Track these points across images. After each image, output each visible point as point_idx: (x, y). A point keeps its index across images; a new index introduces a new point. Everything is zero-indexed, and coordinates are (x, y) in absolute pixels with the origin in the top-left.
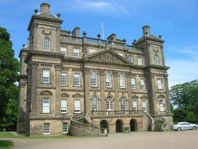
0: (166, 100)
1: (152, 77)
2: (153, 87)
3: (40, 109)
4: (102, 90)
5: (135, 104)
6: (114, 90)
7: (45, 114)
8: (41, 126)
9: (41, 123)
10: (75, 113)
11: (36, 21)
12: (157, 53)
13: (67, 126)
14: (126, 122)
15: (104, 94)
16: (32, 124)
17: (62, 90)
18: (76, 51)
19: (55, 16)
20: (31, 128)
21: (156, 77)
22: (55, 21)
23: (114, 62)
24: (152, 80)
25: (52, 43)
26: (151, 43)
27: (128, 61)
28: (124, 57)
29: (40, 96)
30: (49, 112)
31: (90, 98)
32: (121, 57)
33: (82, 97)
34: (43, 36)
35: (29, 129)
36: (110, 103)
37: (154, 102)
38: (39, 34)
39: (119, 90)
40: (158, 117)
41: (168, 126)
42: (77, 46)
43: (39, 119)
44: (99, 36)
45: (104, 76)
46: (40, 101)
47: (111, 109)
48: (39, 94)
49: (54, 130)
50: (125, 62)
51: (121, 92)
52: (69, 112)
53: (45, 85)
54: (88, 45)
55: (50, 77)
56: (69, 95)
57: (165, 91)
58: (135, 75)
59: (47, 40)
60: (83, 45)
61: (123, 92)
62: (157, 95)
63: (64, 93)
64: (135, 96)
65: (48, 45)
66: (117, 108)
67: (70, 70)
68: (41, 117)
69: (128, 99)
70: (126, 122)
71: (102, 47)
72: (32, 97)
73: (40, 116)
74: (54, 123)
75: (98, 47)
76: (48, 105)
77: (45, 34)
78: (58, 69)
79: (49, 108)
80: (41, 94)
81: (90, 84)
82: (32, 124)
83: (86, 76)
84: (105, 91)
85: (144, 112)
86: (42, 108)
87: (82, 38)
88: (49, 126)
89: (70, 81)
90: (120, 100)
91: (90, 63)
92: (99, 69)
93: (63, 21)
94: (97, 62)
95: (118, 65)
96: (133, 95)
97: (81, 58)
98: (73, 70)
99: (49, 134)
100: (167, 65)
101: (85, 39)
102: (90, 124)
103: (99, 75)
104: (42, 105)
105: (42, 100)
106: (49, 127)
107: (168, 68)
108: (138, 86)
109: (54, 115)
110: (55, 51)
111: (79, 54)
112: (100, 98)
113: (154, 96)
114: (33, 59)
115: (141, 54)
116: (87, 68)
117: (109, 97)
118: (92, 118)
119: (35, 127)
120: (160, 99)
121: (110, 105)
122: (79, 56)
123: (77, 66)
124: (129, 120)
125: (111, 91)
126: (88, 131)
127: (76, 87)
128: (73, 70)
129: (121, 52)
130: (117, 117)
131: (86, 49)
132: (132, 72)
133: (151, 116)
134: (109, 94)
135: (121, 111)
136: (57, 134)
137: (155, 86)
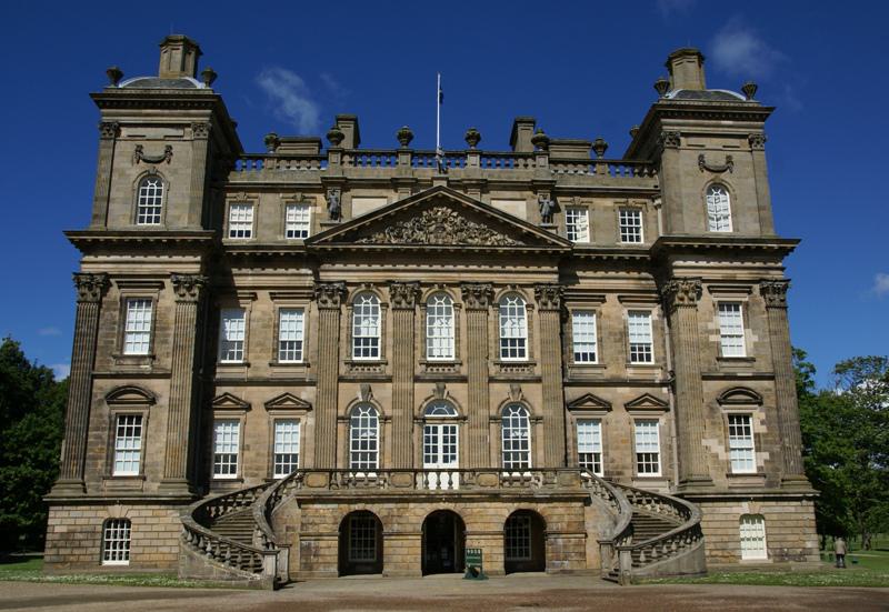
0: (774, 413)
3: (100, 462)
5: (589, 439)
7: (121, 483)
9: (94, 517)
14: (485, 526)
16: (58, 521)
19: (732, 93)
20: (49, 537)
26: (685, 129)
29: (106, 409)
30: (136, 473)
36: (440, 435)
38: (122, 165)
42: (299, 195)
46: (104, 429)
48: (100, 402)
49: (147, 550)
53: (129, 362)
55: (154, 328)
57: (658, 376)
63: (226, 394)
64: (591, 398)
67: (263, 295)
70: (485, 526)
72: (69, 415)
74: (149, 521)
75: (394, 184)
77: (145, 161)
79: (137, 456)
80: (113, 397)
82: (58, 521)
92: (388, 283)
94: (426, 254)
95: (491, 257)
96: (574, 393)
108: (612, 349)
114: (675, 271)
120: (725, 410)
121: (440, 444)
125: (448, 380)
129: (517, 194)
136: (156, 566)
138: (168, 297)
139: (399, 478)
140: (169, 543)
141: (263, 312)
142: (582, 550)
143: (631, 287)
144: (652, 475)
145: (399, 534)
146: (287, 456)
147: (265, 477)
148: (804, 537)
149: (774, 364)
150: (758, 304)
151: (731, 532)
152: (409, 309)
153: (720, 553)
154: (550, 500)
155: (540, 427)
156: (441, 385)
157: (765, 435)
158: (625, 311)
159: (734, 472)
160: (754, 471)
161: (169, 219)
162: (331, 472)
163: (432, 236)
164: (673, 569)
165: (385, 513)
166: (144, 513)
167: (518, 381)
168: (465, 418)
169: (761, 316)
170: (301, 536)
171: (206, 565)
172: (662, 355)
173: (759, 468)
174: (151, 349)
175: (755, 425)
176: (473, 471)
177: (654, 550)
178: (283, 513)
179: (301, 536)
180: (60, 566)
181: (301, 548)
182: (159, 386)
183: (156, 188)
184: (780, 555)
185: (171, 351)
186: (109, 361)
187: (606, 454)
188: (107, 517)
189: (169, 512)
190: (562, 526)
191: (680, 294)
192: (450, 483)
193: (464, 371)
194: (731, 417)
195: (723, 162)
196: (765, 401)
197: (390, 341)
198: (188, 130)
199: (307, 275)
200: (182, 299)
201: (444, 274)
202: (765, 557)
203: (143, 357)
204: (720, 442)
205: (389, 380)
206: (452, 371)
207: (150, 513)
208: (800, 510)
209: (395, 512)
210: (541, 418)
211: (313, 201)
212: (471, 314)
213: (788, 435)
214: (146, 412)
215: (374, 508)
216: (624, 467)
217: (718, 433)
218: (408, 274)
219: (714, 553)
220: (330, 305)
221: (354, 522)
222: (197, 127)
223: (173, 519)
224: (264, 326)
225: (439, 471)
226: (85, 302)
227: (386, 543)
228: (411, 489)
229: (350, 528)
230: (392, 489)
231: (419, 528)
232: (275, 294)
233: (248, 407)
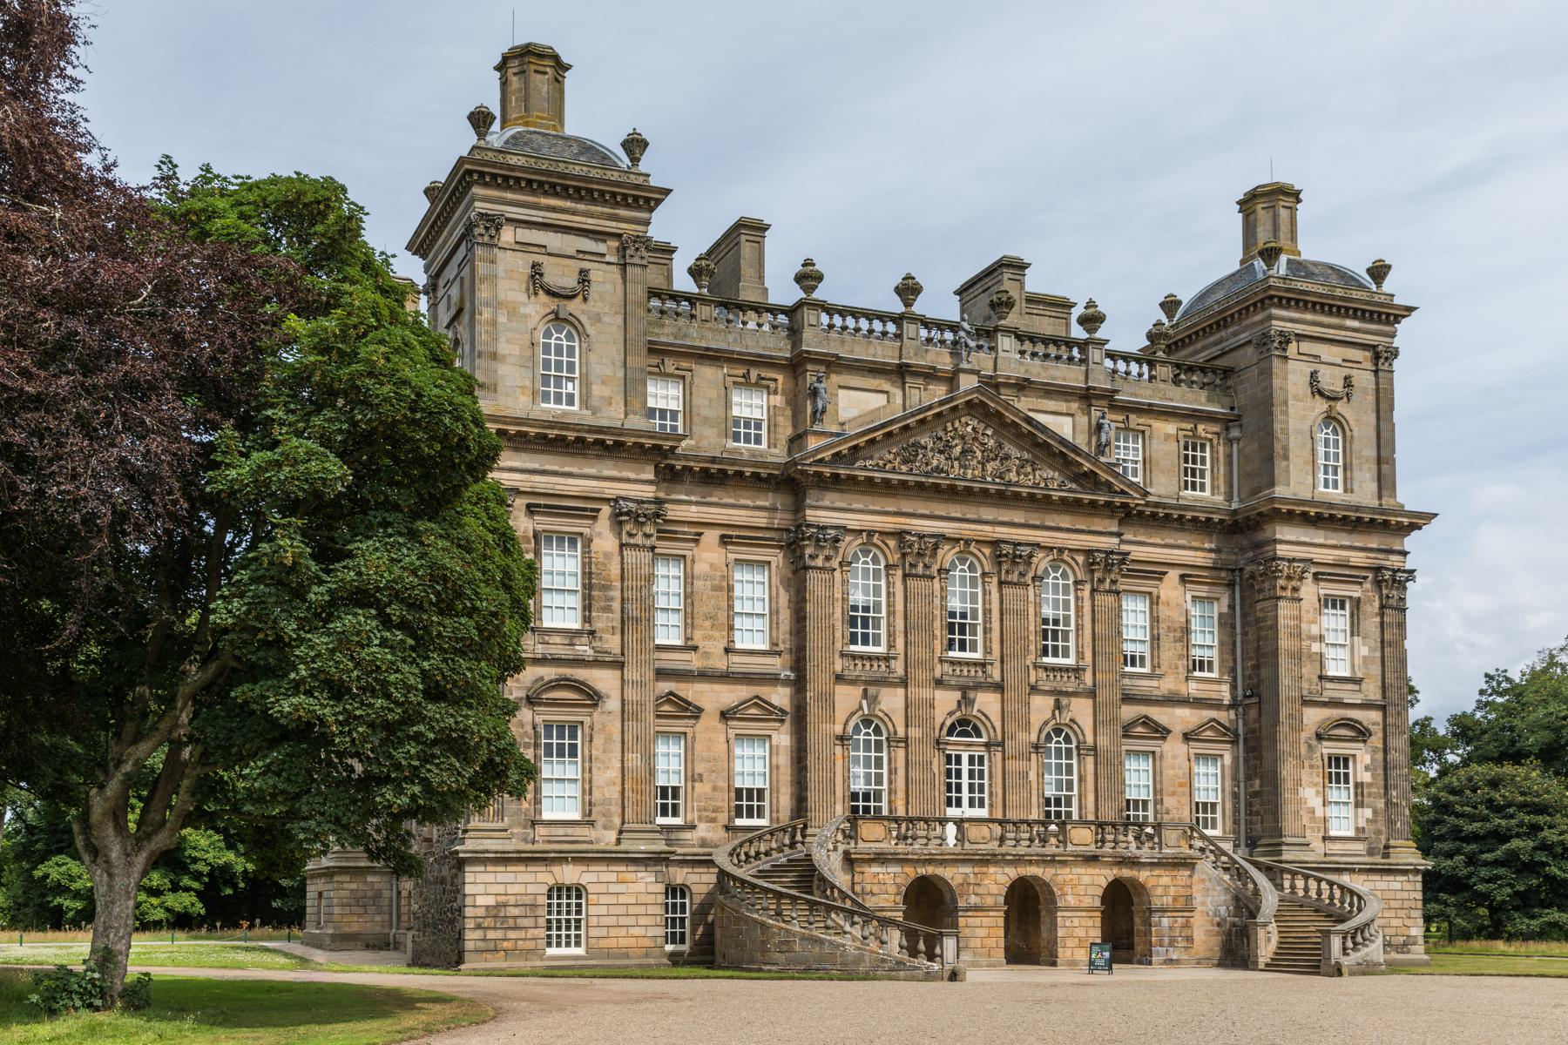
0: (1380, 756)
1: (1283, 588)
2: (1283, 661)
4: (919, 674)
5: (1137, 779)
6: (997, 676)
8: (534, 906)
9: (535, 881)
10: (739, 822)
11: (483, 201)
12: (1340, 407)
13: (683, 905)
15: (932, 706)
16: (479, 889)
17: (661, 674)
18: (750, 405)
20: (469, 912)
21: (1310, 591)
22: (614, 195)
23: (1009, 483)
24: (1285, 610)
25: (593, 358)
26: (1300, 328)
27: (1110, 468)
28: (1081, 441)
30: (576, 816)
31: (838, 729)
32: (1063, 441)
33: (782, 721)
34: (537, 308)
35: (452, 922)
36: (965, 767)
37: (1287, 771)
39: (1033, 680)
40: (1306, 877)
41: (1379, 941)
42: (754, 374)
43: (520, 860)
45: (936, 581)
47: (971, 805)
49: (613, 932)
50: (1089, 480)
51: (1047, 693)
52: (700, 819)
53: (558, 639)
54: (834, 364)
55: (588, 587)
56: (700, 710)
58: (1155, 572)
59: (559, 338)
60: (796, 365)
61: (1058, 693)
62: (1314, 717)
64: (1147, 721)
65: (571, 366)
66: (1012, 798)
67: (711, 536)
68: (529, 847)
69: (1090, 740)
71: (931, 375)
73: (525, 841)
74: (614, 888)
75: (901, 373)
76: (571, 770)
77: (549, 292)
79: (574, 790)
81: (838, 634)
82: (479, 889)
83: (814, 580)
84: (939, 683)
85: (1203, 837)
87: (792, 311)
88: (579, 905)
90: (1036, 747)
91: (842, 491)
92: (900, 535)
93: (667, 192)
95: (1039, 502)
96: (1129, 712)
97: (779, 455)
98: (725, 541)
99: (581, 951)
100: (1409, 496)
101: (809, 316)
102: (844, 896)
103: (899, 573)
106: (579, 912)
107: (1417, 521)
108: (1169, 652)
109: (612, 836)
110: (612, 415)
111: (765, 426)
112: (901, 732)
113: (1284, 728)
115: (1209, 418)
116: (824, 528)
117: (963, 722)
118: (849, 861)
119: (498, 906)
120: (1328, 748)
121: (965, 781)
122: (764, 446)
123: (750, 511)
124: (1097, 879)
125: (978, 687)
126: (838, 939)
128: (725, 541)
129: (1062, 406)
130: (1018, 860)
131: (814, 393)
132: (1138, 552)
133: (1256, 865)
134: (966, 701)
135: (1044, 824)
136: (627, 956)
137: (1298, 657)
140: (643, 921)
143: (1200, 562)
145: (977, 908)
146: (750, 791)
147: (726, 822)
148: (1407, 922)
159: (1332, 833)
165: (959, 879)
166: (605, 877)
174: (587, 619)
180: (489, 956)
182: (604, 680)
188: (551, 882)
189: (640, 875)
190: (1167, 901)
191: (1281, 582)
201: (973, 526)
207: (613, 877)
209: (972, 879)
211: (772, 385)
213: (1396, 787)
218: (926, 521)
220: (639, 540)
224: (715, 588)
231: (1001, 900)
232: (731, 537)
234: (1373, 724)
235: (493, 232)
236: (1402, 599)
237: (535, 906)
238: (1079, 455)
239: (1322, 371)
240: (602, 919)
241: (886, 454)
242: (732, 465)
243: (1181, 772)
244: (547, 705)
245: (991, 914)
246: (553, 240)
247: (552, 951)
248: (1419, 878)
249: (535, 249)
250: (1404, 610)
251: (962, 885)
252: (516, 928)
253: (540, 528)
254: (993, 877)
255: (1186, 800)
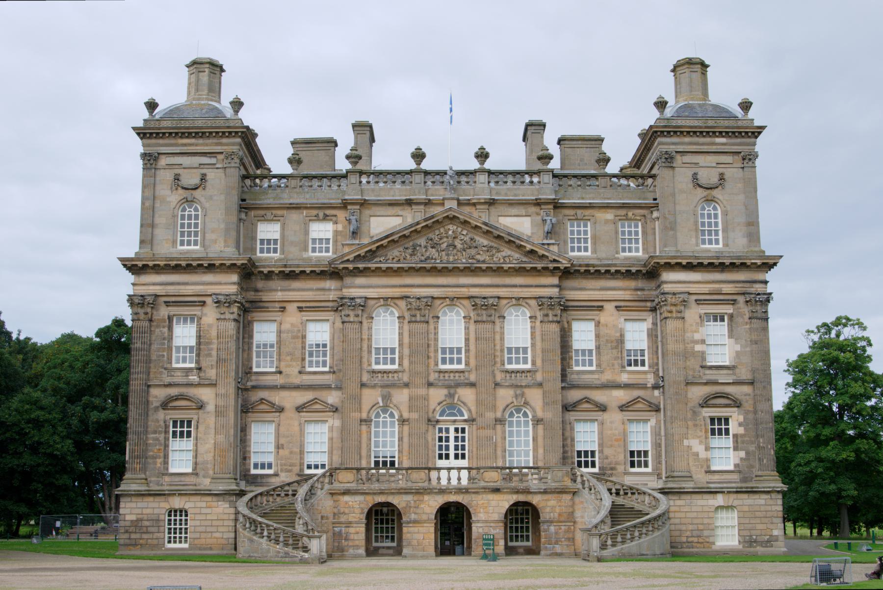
0: (751, 416)
7: (177, 479)
8: (158, 520)
9: (158, 508)
18: (322, 230)
26: (680, 148)
29: (161, 415)
30: (189, 470)
44: (419, 156)
46: (160, 432)
48: (156, 409)
49: (203, 535)
55: (199, 343)
64: (588, 400)
67: (292, 308)
73: (158, 484)
74: (204, 511)
76: (187, 444)
78: (228, 316)
79: (190, 456)
80: (165, 405)
86: (166, 457)
89: (290, 354)
98: (300, 309)
99: (186, 546)
100: (769, 249)
104: (166, 446)
105: (167, 427)
108: (608, 355)
116: (353, 299)
119: (138, 520)
120: (708, 413)
122: (721, 246)
127: (315, 373)
136: (211, 549)
138: (210, 315)
139: (415, 475)
140: (221, 529)
141: (292, 325)
142: (571, 536)
144: (643, 470)
145: (415, 522)
149: (753, 371)
150: (742, 315)
151: (706, 521)
152: (423, 322)
153: (695, 540)
154: (545, 492)
155: (540, 428)
156: (452, 391)
157: (742, 436)
158: (622, 320)
159: (713, 468)
160: (731, 468)
161: (207, 243)
162: (358, 470)
163: (444, 253)
164: (635, 551)
165: (408, 506)
167: (521, 386)
168: (473, 420)
169: (743, 329)
170: (333, 523)
171: (264, 546)
172: (655, 361)
173: (736, 465)
174: (198, 362)
175: (734, 427)
176: (478, 469)
177: (628, 533)
178: (318, 504)
179: (333, 523)
181: (334, 534)
182: (206, 394)
183: (193, 213)
184: (749, 541)
185: (214, 363)
186: (161, 373)
187: (601, 451)
188: (168, 507)
189: (220, 503)
192: (459, 479)
193: (473, 378)
194: (712, 420)
195: (715, 180)
196: (745, 404)
197: (406, 351)
198: (220, 157)
199: (330, 290)
200: (222, 317)
201: (454, 289)
202: (737, 543)
203: (191, 369)
204: (701, 442)
205: (407, 385)
206: (462, 378)
207: (204, 504)
208: (771, 502)
210: (542, 420)
211: (334, 219)
212: (480, 326)
213: (763, 436)
214: (195, 417)
215: (395, 500)
216: (617, 463)
217: (700, 434)
219: (690, 539)
221: (376, 512)
222: (230, 156)
223: (223, 508)
224: (294, 337)
225: (449, 469)
226: (139, 320)
227: (405, 530)
228: (426, 484)
229: (374, 517)
230: (410, 484)
233: (281, 410)
234: (746, 395)
235: (152, 161)
236: (766, 312)
237: (158, 520)
238: (522, 241)
239: (700, 173)
240: (197, 528)
241: (395, 252)
242: (298, 267)
243: (617, 432)
244: (171, 409)
245: (425, 525)
246: (186, 161)
247: (172, 545)
248: (780, 496)
249: (177, 167)
250: (767, 319)
251: (405, 508)
252: (147, 532)
253: (172, 313)
254: (427, 503)
255: (621, 450)
